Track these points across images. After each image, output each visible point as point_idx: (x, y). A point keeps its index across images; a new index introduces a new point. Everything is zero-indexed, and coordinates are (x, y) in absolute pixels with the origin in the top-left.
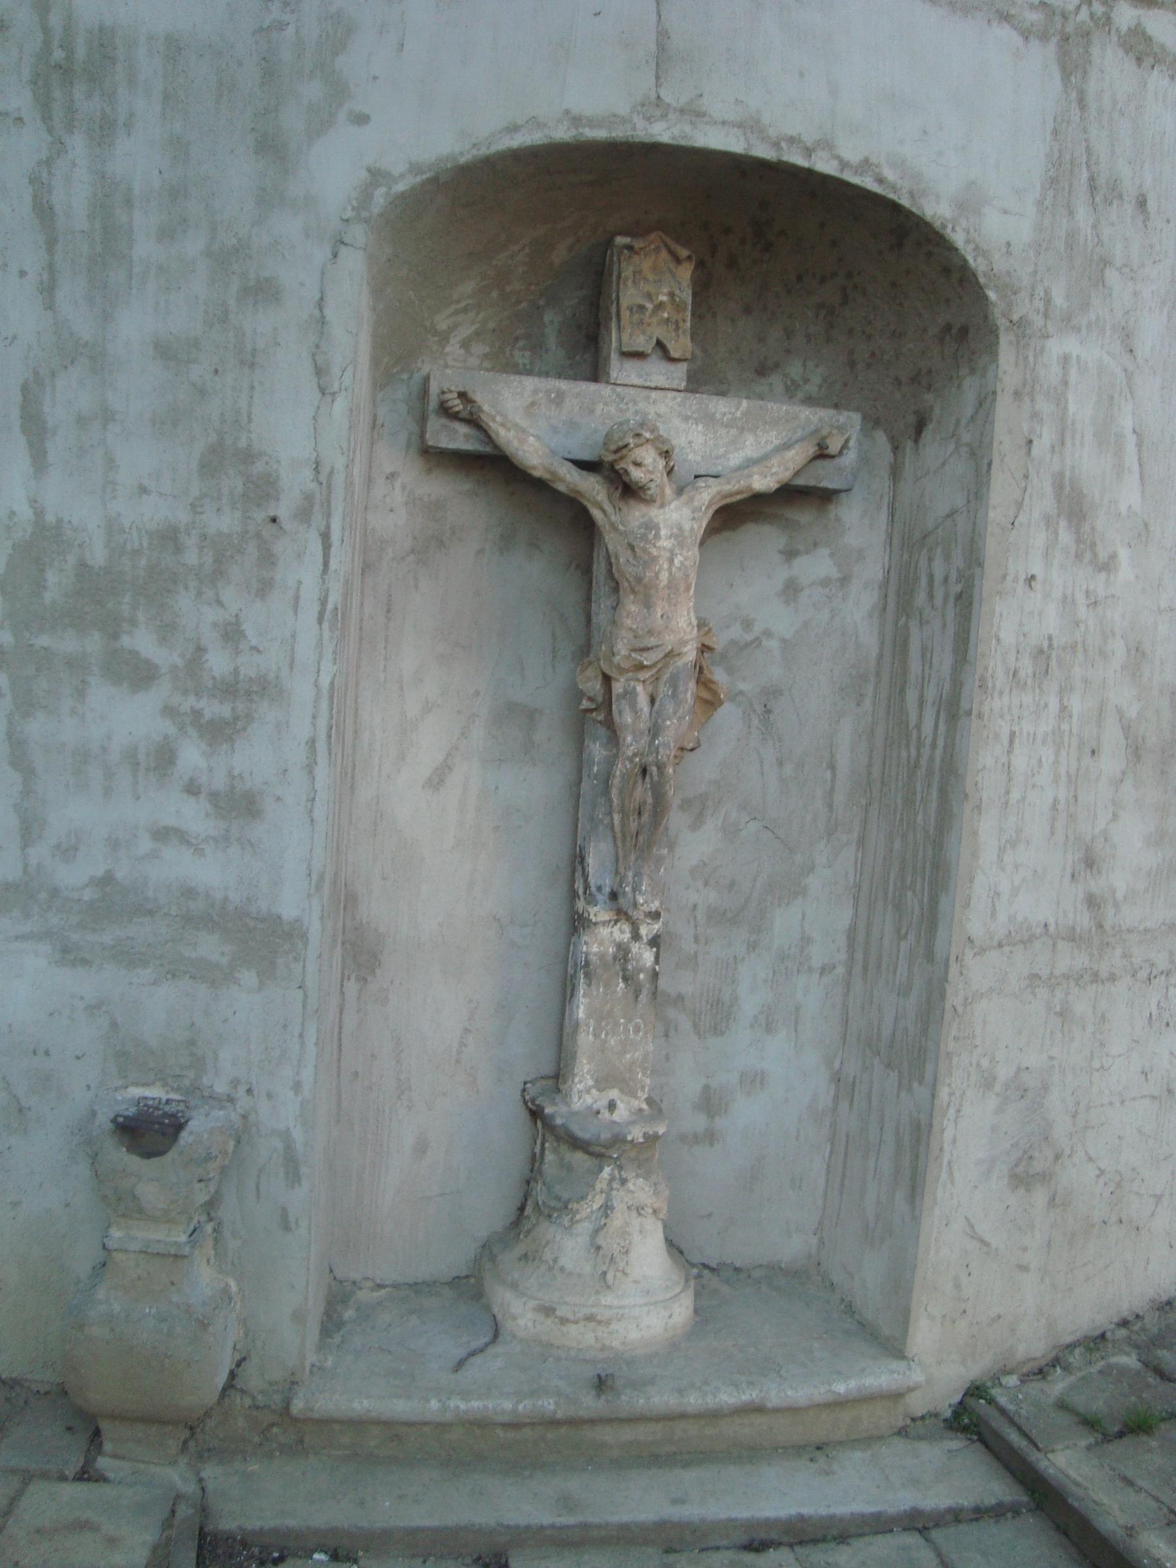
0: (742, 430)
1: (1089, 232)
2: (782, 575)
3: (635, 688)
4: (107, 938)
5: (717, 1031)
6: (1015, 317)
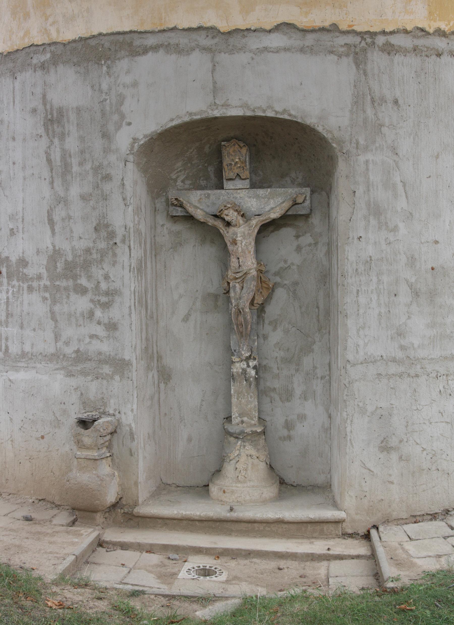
0: (269, 199)
1: (373, 117)
2: (295, 244)
3: (235, 285)
4: (79, 368)
5: (288, 400)
6: (344, 151)
